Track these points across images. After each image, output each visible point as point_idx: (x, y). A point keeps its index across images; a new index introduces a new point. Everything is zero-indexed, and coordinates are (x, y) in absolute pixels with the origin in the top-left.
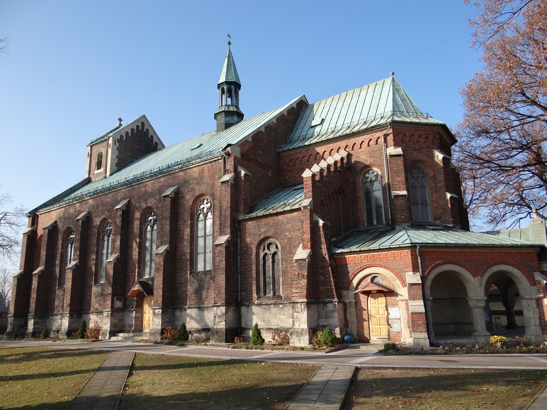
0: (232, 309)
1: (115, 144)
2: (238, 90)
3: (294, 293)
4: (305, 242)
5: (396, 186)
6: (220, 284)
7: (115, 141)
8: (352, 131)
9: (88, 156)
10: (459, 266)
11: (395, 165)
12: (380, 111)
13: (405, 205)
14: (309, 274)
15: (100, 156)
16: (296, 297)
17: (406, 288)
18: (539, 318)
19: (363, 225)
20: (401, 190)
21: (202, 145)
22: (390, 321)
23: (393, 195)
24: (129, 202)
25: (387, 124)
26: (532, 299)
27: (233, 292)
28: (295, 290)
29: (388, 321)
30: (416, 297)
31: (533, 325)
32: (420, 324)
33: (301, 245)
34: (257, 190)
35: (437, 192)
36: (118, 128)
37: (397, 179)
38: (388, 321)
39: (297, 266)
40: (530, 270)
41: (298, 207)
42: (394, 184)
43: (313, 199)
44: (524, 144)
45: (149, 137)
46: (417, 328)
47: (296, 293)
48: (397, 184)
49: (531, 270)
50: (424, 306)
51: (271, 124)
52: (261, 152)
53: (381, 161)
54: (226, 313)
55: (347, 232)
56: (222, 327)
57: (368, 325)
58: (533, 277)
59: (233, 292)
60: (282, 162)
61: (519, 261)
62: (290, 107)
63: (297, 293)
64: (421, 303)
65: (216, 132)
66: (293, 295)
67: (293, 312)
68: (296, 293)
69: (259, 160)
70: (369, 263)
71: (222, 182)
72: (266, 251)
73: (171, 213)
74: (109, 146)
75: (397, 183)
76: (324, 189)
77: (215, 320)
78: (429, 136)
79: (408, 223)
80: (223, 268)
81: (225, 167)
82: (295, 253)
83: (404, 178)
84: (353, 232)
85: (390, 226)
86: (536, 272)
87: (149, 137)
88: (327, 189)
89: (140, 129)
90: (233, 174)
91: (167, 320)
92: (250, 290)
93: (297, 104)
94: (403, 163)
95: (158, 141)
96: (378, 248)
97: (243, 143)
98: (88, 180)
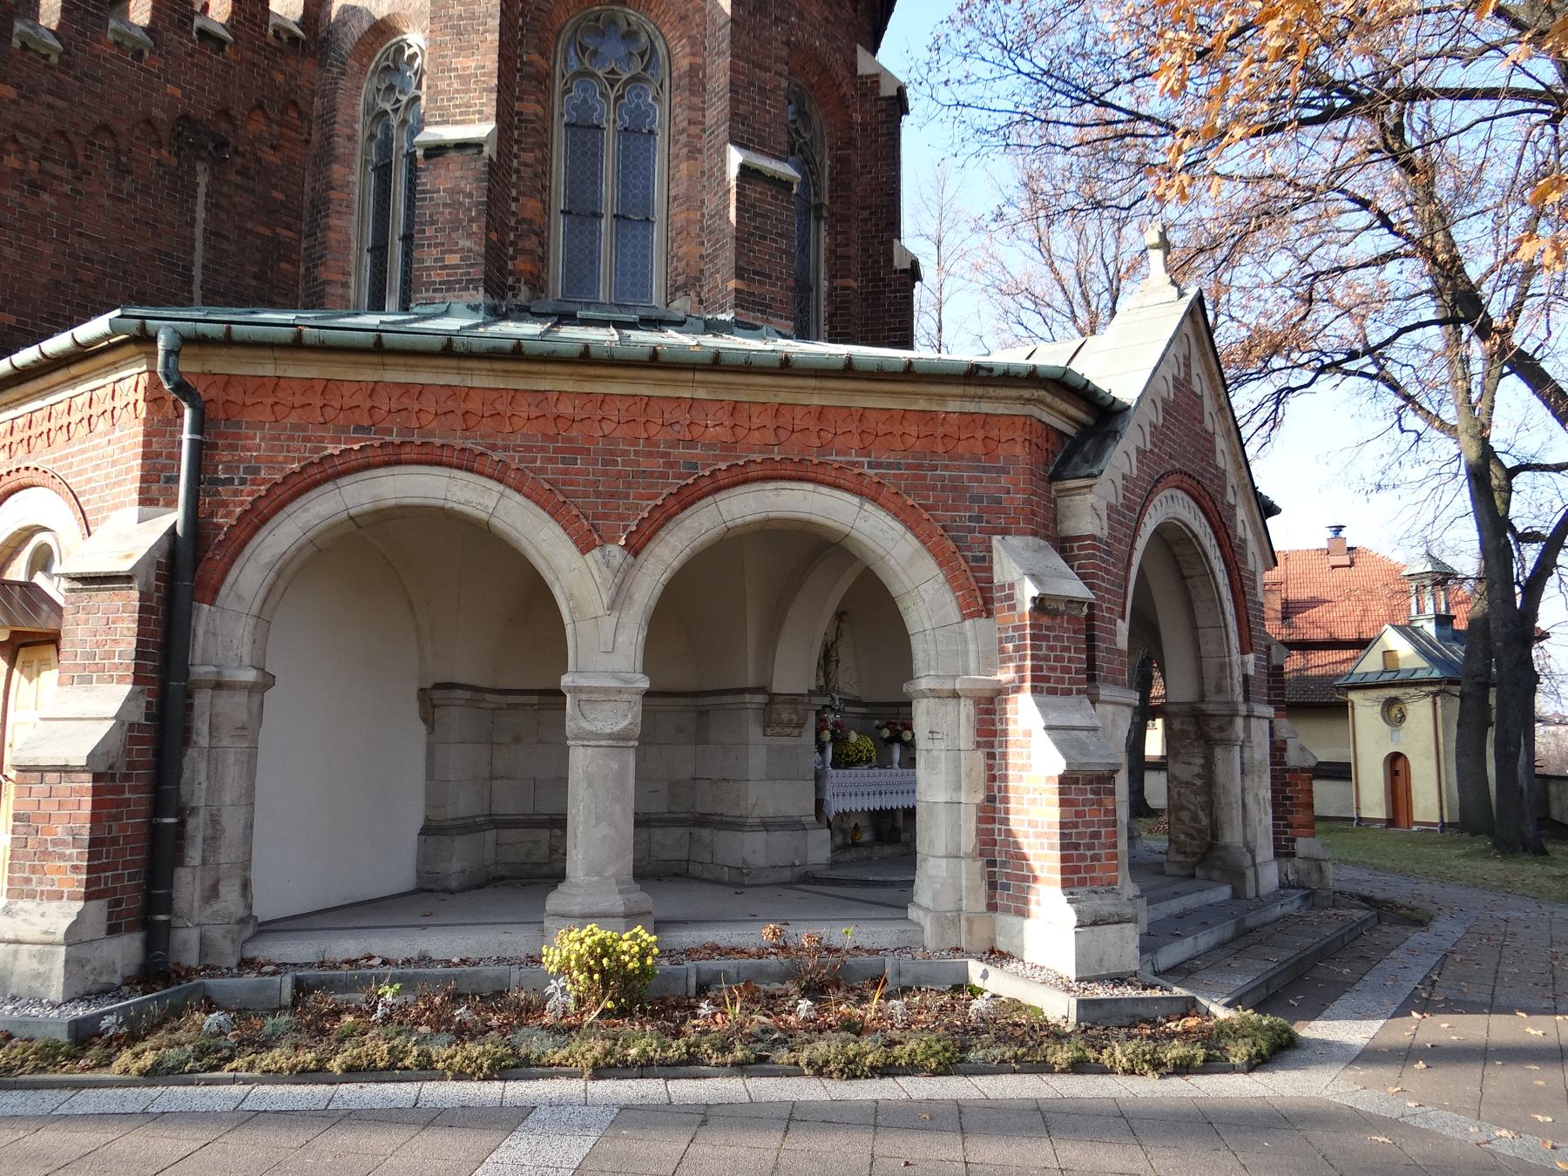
5: (449, 100)
10: (490, 477)
13: (470, 195)
26: (955, 695)
31: (943, 852)
32: (55, 843)
35: (700, 151)
37: (458, 62)
40: (971, 519)
46: (33, 870)
48: (457, 91)
49: (978, 519)
58: (983, 564)
61: (908, 467)
79: (476, 288)
86: (1004, 532)
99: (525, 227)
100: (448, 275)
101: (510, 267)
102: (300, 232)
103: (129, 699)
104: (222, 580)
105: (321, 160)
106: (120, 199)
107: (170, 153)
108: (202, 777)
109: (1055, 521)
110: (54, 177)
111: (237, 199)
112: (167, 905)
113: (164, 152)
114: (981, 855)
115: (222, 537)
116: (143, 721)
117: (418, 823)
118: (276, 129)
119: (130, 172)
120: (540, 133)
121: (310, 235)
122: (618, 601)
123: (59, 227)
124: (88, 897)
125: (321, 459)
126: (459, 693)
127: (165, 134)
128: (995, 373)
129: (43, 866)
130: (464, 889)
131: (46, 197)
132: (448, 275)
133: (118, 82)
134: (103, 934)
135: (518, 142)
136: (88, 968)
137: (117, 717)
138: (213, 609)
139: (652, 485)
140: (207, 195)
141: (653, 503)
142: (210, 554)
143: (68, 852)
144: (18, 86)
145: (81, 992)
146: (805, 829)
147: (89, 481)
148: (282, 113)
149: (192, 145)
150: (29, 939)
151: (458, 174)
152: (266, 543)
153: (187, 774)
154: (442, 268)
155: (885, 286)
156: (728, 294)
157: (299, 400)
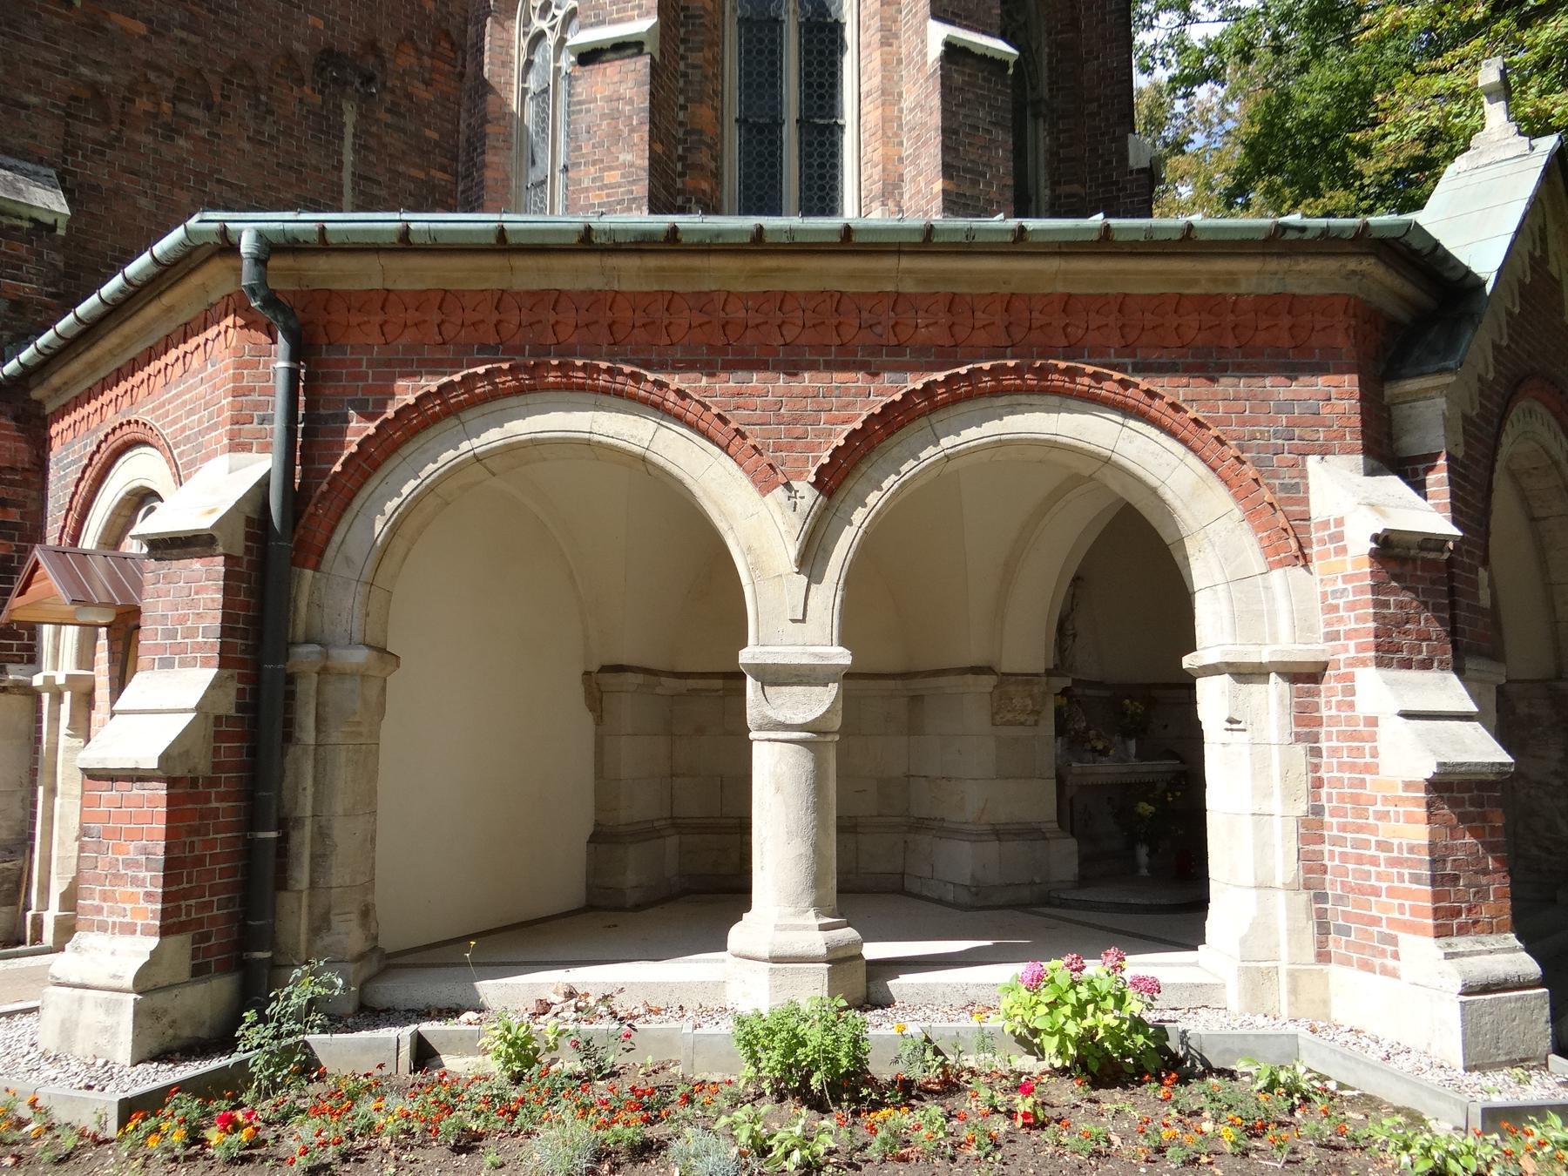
13: (631, 101)
18: (1304, 823)
32: (128, 864)
46: (105, 897)
58: (1297, 491)
79: (639, 208)
86: (1324, 452)
99: (695, 137)
100: (608, 196)
101: (679, 185)
102: (456, 174)
103: (213, 686)
104: (328, 540)
105: (477, 93)
106: (261, 143)
107: (313, 89)
108: (309, 782)
109: (1390, 436)
110: (190, 119)
111: (387, 139)
112: (269, 938)
113: (307, 89)
114: (1307, 888)
115: (324, 487)
116: (233, 712)
117: (587, 829)
118: (427, 61)
119: (271, 113)
120: (709, 30)
121: (467, 177)
122: (811, 558)
123: (197, 174)
124: (165, 931)
125: (441, 388)
126: (631, 678)
127: (307, 71)
128: (1308, 235)
129: (114, 892)
130: (638, 907)
131: (181, 142)
132: (608, 196)
133: (255, 14)
134: (185, 974)
135: (684, 41)
136: (165, 1021)
137: (198, 708)
138: (318, 575)
139: (846, 406)
140: (355, 135)
141: (848, 428)
142: (311, 509)
143: (141, 875)
144: (148, 21)
145: (156, 1050)
146: (1045, 839)
147: (183, 429)
148: (434, 44)
149: (335, 80)
150: (95, 983)
151: (616, 79)
152: (375, 495)
153: (289, 779)
154: (601, 188)
155: (1119, 190)
156: (934, 199)
157: (413, 315)
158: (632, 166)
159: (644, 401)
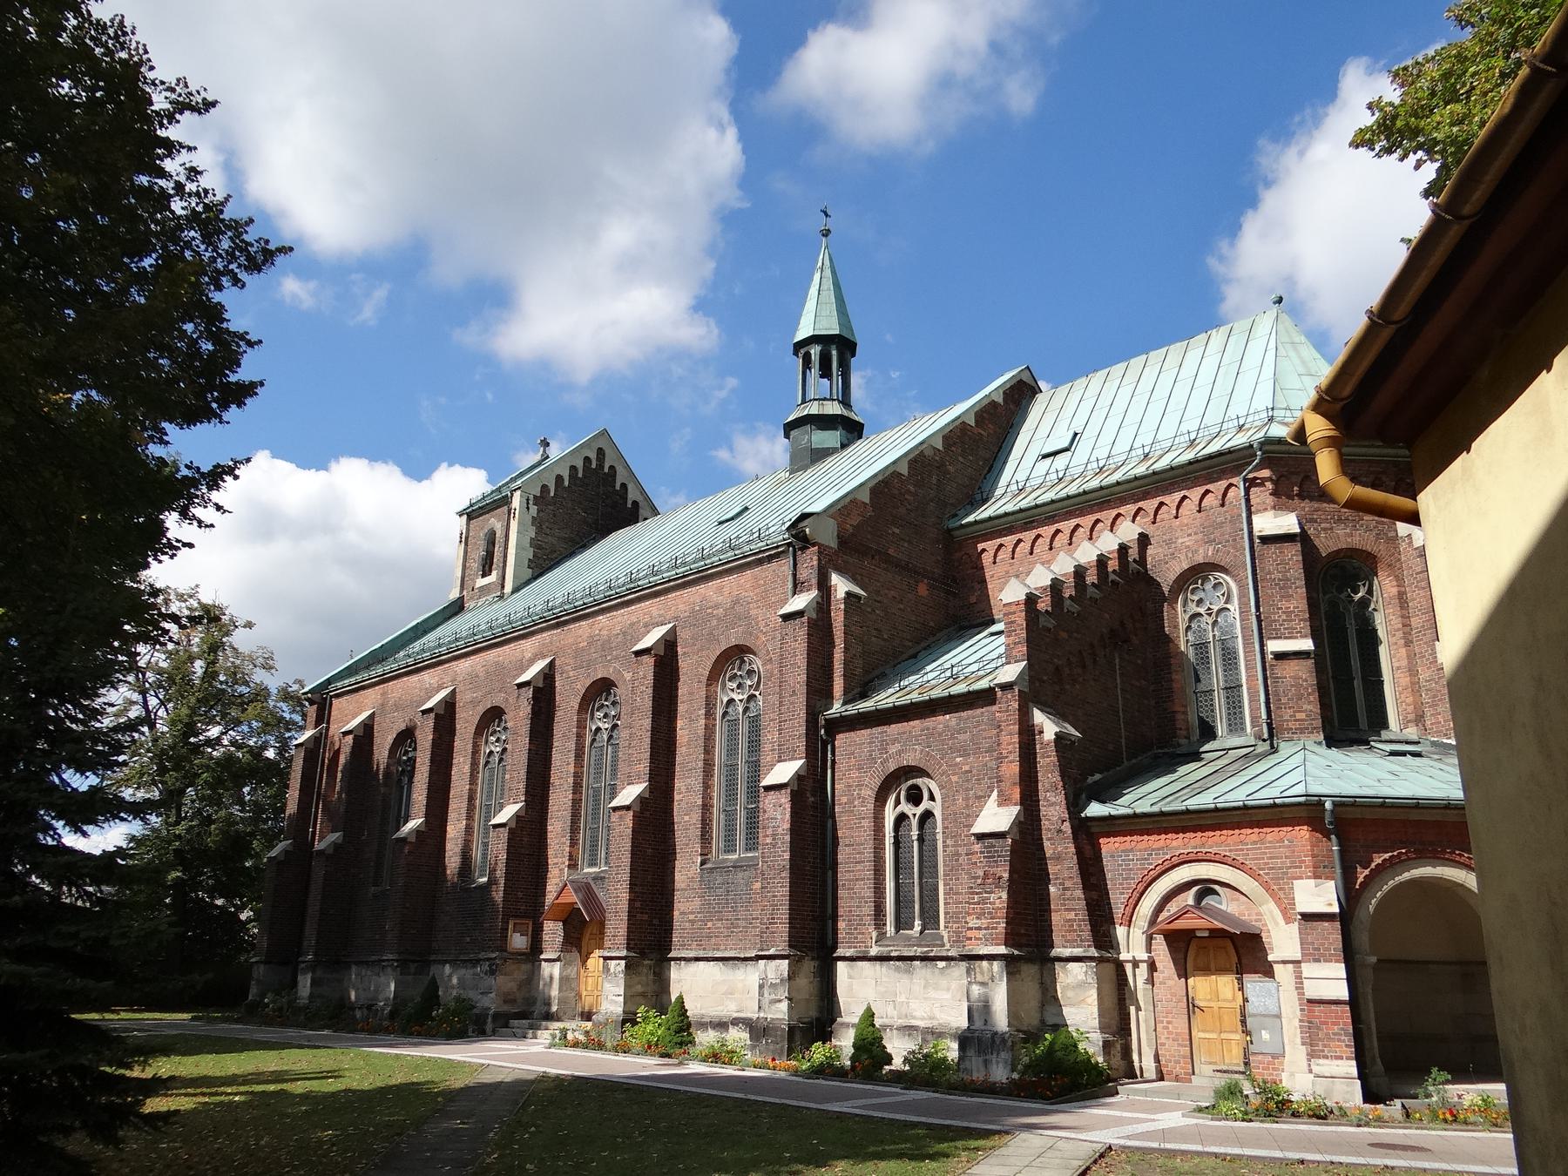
0: (809, 966)
1: (528, 508)
2: (849, 355)
3: (971, 929)
4: (1005, 785)
5: (1281, 625)
6: (774, 896)
7: (528, 500)
8: (1083, 487)
9: (461, 542)
11: (1277, 565)
12: (1238, 408)
14: (1016, 876)
15: (491, 539)
16: (976, 939)
17: (1295, 926)
19: (1188, 738)
20: (1296, 638)
21: (746, 509)
22: (1249, 1020)
23: (1272, 652)
24: (552, 665)
25: (1251, 446)
27: (811, 920)
28: (975, 921)
29: (1244, 1022)
30: (1324, 955)
33: (995, 793)
34: (886, 637)
36: (539, 464)
37: (1284, 604)
38: (1244, 1022)
39: (982, 852)
41: (987, 686)
42: (1275, 621)
43: (1030, 666)
44: (190, 789)
45: (618, 487)
46: (1325, 1046)
47: (977, 929)
48: (1284, 620)
50: (1348, 982)
51: (928, 453)
52: (897, 531)
53: (1238, 554)
54: (790, 978)
55: (1140, 758)
56: (780, 1016)
57: (1187, 1031)
59: (811, 920)
60: (958, 555)
62: (986, 402)
63: (979, 929)
64: (1340, 970)
65: (788, 473)
66: (970, 934)
67: (970, 983)
68: (977, 929)
69: (891, 552)
70: (1188, 848)
71: (781, 616)
72: (905, 807)
73: (653, 697)
74: (512, 515)
75: (1284, 617)
76: (1064, 635)
77: (761, 994)
78: (1384, 479)
79: (1318, 732)
80: (784, 851)
81: (795, 575)
82: (978, 816)
83: (1305, 601)
84: (1156, 757)
85: (1264, 740)
87: (618, 487)
88: (1075, 635)
89: (594, 466)
90: (814, 593)
91: (639, 988)
92: (857, 916)
93: (1004, 393)
94: (1300, 558)
95: (639, 499)
96: (1213, 806)
97: (843, 509)
98: (459, 603)
132: (1299, 724)
158: (1311, 711)
159: (1463, 864)
